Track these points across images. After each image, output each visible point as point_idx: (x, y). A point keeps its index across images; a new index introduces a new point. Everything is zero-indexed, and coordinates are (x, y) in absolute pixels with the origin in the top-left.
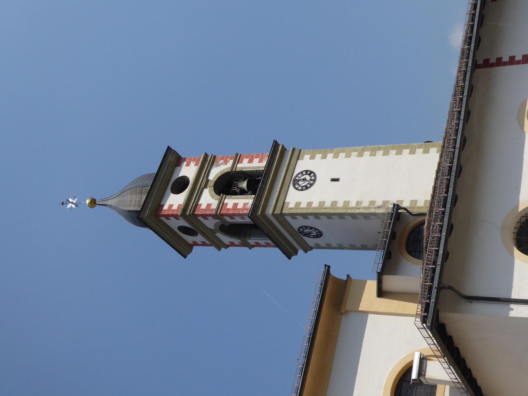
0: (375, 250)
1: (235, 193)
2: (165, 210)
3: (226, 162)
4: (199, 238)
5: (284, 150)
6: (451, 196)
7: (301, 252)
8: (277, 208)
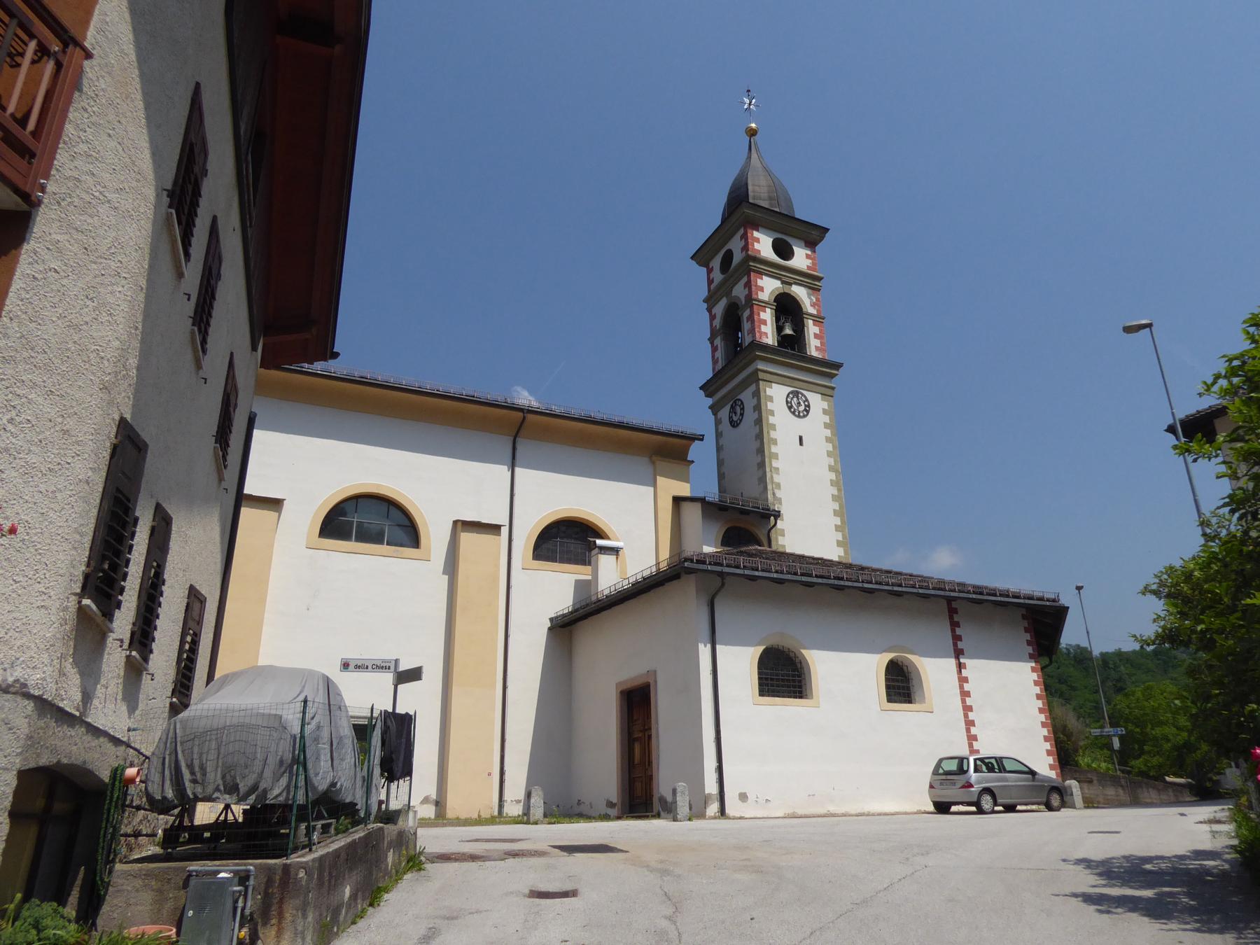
0: (720, 492)
1: (778, 320)
2: (752, 234)
3: (813, 305)
4: (718, 276)
5: (832, 376)
6: (814, 581)
7: (710, 401)
8: (765, 374)
